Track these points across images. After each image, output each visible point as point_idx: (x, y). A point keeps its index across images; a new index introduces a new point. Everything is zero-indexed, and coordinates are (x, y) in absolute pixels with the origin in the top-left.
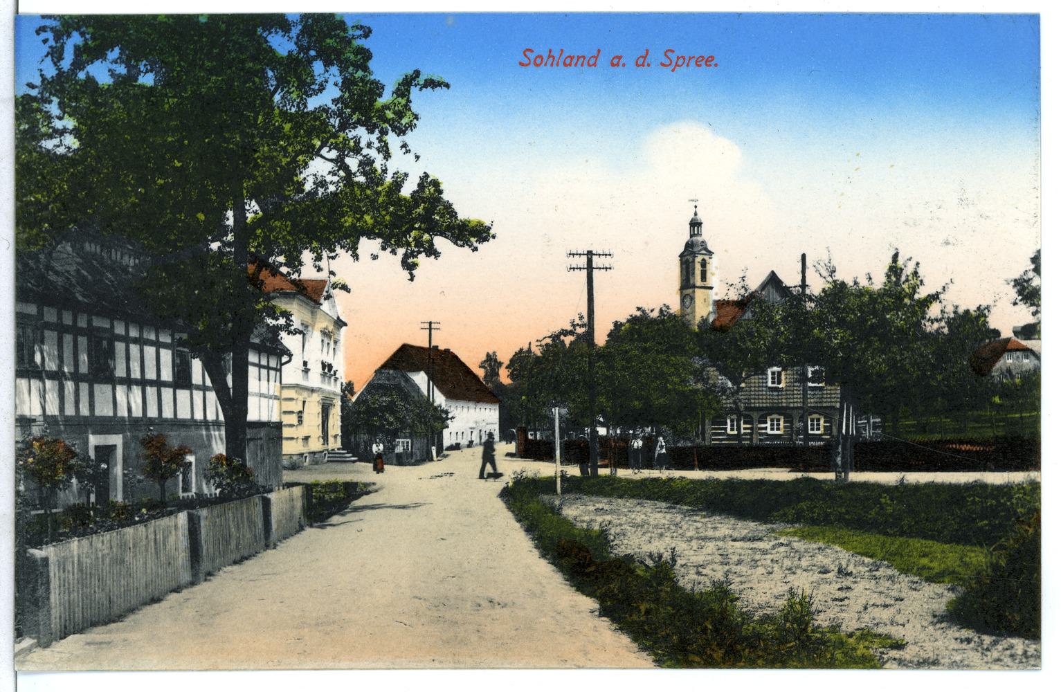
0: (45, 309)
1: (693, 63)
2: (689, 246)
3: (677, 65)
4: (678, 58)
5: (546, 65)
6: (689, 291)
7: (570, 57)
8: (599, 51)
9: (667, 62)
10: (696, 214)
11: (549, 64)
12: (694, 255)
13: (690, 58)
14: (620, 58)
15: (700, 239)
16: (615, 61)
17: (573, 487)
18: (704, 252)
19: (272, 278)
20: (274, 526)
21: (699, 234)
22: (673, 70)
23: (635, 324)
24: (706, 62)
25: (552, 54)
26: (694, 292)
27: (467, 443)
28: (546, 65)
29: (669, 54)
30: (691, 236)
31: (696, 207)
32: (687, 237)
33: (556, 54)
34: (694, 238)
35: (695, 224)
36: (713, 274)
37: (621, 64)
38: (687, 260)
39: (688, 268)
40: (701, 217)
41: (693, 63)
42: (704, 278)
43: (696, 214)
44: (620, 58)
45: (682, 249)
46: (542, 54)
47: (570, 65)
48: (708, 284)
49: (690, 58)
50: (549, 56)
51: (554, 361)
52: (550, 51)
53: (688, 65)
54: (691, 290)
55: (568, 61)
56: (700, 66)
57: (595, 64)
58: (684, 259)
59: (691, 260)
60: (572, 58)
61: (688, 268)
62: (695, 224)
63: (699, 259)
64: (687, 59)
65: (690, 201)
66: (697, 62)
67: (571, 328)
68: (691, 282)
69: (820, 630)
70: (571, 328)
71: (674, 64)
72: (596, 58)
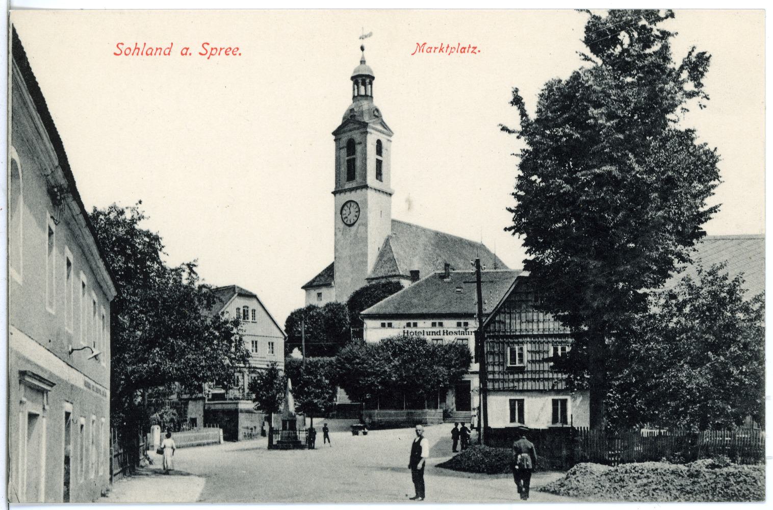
0: (346, 149)
1: (223, 52)
3: (211, 54)
4: (212, 49)
5: (133, 54)
7: (429, 48)
8: (172, 44)
9: (204, 52)
10: (363, 62)
11: (135, 54)
13: (221, 49)
14: (187, 49)
16: (184, 52)
19: (322, 302)
20: (476, 290)
21: (368, 97)
22: (208, 58)
23: (486, 457)
24: (233, 51)
25: (138, 46)
28: (133, 54)
29: (206, 46)
31: (362, 49)
33: (141, 46)
35: (362, 80)
36: (440, 428)
37: (188, 53)
40: (374, 66)
41: (223, 52)
42: (379, 174)
43: (363, 62)
44: (187, 49)
45: (339, 122)
46: (130, 46)
47: (186, 54)
49: (221, 49)
53: (219, 54)
55: (149, 52)
56: (228, 54)
57: (169, 54)
58: (345, 138)
60: (464, 48)
62: (362, 80)
64: (155, 50)
65: (370, 35)
66: (226, 52)
71: (209, 53)
72: (170, 49)
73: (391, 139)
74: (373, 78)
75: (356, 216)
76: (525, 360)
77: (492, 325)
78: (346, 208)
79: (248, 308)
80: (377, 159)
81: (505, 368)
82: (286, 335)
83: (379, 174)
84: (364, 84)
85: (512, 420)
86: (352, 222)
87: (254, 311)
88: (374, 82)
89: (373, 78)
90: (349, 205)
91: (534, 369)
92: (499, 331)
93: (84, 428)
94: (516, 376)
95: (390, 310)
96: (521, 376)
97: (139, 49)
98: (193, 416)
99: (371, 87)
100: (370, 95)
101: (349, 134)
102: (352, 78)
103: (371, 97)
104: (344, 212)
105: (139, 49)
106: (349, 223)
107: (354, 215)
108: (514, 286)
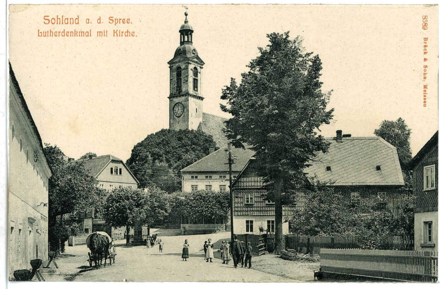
2: (180, 53)
6: (182, 99)
8: (78, 16)
12: (187, 61)
15: (192, 47)
17: (239, 174)
18: (196, 60)
21: (190, 42)
26: (187, 100)
27: (335, 135)
30: (182, 43)
31: (186, 15)
32: (177, 45)
33: (60, 17)
34: (186, 46)
35: (186, 32)
38: (179, 68)
39: (179, 75)
40: (191, 25)
42: (195, 87)
45: (172, 57)
48: (200, 93)
50: (58, 19)
51: (208, 208)
52: (57, 16)
54: (183, 98)
58: (175, 66)
59: (183, 67)
61: (179, 75)
62: (186, 32)
63: (191, 66)
67: (288, 223)
68: (184, 89)
69: (20, 96)
70: (288, 223)
73: (203, 66)
74: (192, 31)
75: (182, 112)
76: (254, 201)
77: (237, 183)
78: (176, 107)
79: (117, 167)
80: (197, 77)
81: (244, 205)
82: (139, 182)
83: (195, 87)
84: (187, 35)
85: (247, 231)
86: (180, 115)
87: (120, 169)
88: (193, 34)
89: (192, 31)
90: (177, 105)
91: (258, 206)
92: (238, 187)
93: (22, 231)
94: (271, 208)
95: (194, 169)
96: (251, 209)
97: (60, 19)
98: (87, 228)
99: (191, 37)
100: (190, 41)
101: (177, 64)
102: (180, 31)
103: (191, 42)
104: (175, 109)
105: (60, 19)
106: (178, 115)
107: (181, 111)
108: (247, 165)
